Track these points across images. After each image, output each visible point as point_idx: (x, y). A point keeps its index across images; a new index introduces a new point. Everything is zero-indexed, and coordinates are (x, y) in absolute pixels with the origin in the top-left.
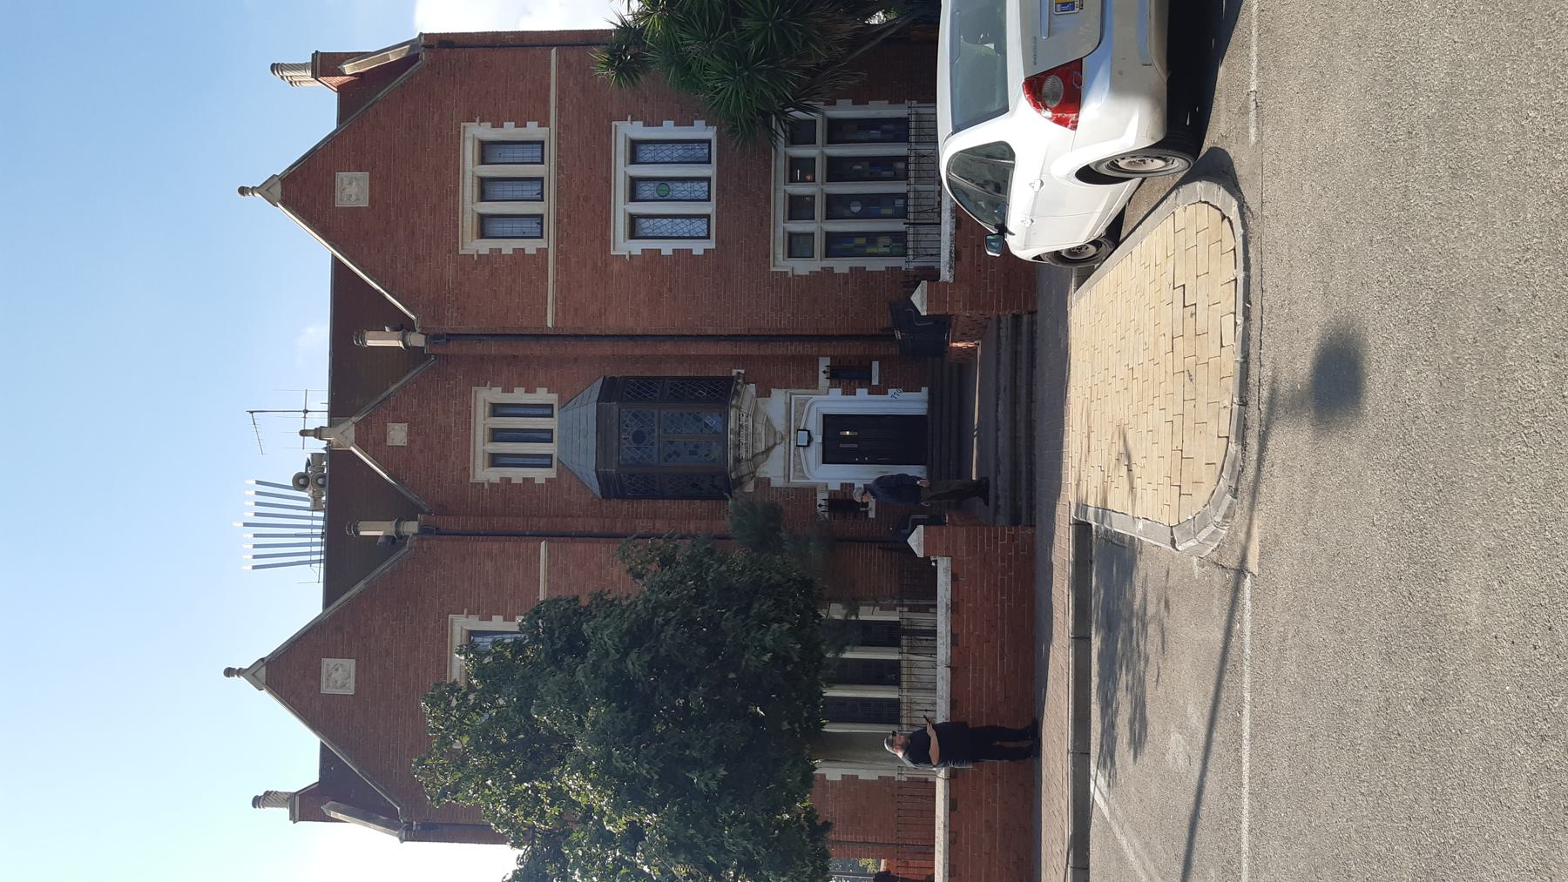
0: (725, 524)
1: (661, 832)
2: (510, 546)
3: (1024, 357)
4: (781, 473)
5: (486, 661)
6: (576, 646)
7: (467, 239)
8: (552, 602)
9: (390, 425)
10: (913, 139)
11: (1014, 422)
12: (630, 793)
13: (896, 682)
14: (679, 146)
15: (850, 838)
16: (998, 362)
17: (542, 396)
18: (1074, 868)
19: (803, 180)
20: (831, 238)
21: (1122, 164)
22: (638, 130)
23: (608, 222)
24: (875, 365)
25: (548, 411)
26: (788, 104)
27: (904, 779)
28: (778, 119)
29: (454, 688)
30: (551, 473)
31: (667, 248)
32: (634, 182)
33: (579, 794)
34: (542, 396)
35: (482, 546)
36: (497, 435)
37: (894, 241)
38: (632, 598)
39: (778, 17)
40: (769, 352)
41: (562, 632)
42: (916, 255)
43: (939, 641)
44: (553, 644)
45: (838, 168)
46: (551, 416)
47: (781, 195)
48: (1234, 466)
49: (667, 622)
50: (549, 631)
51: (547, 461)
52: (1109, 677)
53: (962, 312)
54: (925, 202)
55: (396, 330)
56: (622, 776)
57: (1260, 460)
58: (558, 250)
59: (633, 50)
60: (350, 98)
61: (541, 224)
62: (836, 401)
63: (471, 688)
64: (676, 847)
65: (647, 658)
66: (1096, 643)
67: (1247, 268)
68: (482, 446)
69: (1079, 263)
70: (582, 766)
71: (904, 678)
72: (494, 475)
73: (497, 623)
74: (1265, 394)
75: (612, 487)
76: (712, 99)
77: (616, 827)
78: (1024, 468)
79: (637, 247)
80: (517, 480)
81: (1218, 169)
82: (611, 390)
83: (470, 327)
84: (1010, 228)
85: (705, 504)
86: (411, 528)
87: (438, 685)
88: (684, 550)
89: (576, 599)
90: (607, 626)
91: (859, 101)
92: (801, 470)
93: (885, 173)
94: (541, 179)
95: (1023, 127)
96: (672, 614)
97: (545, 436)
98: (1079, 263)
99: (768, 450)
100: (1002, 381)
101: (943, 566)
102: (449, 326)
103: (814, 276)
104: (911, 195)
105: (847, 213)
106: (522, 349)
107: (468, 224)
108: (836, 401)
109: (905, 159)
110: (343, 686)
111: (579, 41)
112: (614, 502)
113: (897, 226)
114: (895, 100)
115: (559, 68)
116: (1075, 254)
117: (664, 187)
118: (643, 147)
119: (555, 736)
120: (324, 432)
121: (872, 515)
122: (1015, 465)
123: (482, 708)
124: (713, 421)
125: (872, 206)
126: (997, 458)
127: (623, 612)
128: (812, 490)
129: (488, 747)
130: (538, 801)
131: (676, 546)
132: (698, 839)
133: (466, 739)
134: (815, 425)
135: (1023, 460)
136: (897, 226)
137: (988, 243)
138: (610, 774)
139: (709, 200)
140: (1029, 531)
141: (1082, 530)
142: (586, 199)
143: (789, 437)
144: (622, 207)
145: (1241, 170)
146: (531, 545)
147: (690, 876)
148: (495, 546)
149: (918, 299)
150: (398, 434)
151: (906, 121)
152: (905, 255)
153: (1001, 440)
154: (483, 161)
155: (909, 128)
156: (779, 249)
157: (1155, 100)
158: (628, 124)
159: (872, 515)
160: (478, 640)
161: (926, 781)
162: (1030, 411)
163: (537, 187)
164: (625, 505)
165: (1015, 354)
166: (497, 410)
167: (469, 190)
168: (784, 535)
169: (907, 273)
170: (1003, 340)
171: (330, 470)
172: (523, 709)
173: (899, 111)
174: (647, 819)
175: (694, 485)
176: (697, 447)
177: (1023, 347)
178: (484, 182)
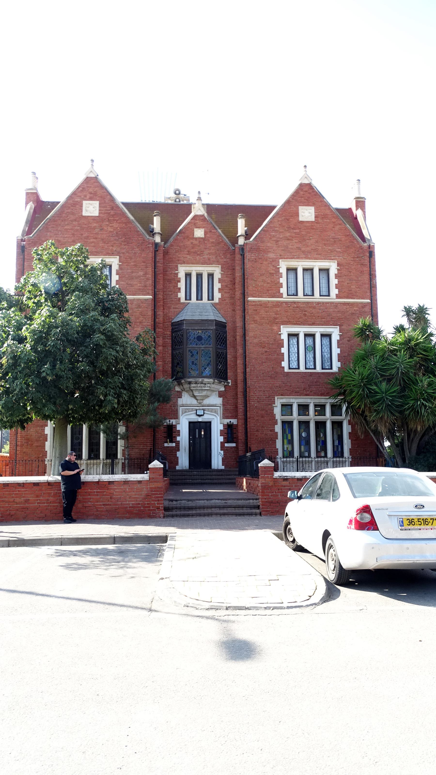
0: (161, 378)
1: (22, 352)
2: (150, 282)
3: (241, 511)
5: (99, 272)
6: (106, 311)
7: (287, 263)
8: (126, 301)
10: (335, 459)
11: (211, 507)
12: (40, 338)
13: (90, 458)
14: (329, 355)
15: (19, 438)
16: (238, 499)
17: (217, 296)
18: (9, 541)
19: (316, 411)
20: (291, 423)
21: (332, 550)
22: (336, 337)
23: (295, 324)
24: (234, 445)
25: (210, 298)
26: (349, 403)
27: (46, 463)
28: (342, 399)
29: (86, 258)
31: (284, 350)
32: (313, 336)
33: (39, 314)
34: (217, 296)
35: (150, 270)
36: (199, 276)
37: (290, 452)
38: (127, 336)
39: (387, 399)
40: (239, 396)
41: (111, 306)
42: (283, 462)
43: (111, 476)
44: (107, 301)
45: (320, 426)
46: (208, 300)
47: (309, 401)
48: (198, 605)
49: (117, 352)
50: (113, 300)
51: (188, 298)
52: (97, 553)
53: (259, 483)
54: (307, 465)
55: (246, 232)
56: (48, 333)
57: (202, 617)
58: (282, 303)
59: (371, 335)
60: (347, 214)
61: (294, 295)
62: (217, 427)
63: (86, 266)
64: (15, 359)
65: (101, 343)
66: (111, 547)
67: (288, 608)
68: (194, 270)
69: (285, 533)
70: (52, 315)
71: (92, 461)
72: (182, 275)
73: (115, 277)
74: (232, 618)
75: (177, 328)
76: (351, 369)
77: (24, 332)
78: (190, 512)
79: (284, 337)
81: (331, 594)
82: (221, 326)
83: (248, 265)
84: (300, 501)
85: (170, 369)
86: (158, 239)
87: (87, 251)
88: (150, 359)
89: (127, 311)
90: (115, 325)
91: (351, 435)
92: (185, 412)
93: (319, 447)
94: (313, 295)
95: (347, 505)
96: (121, 354)
97: (199, 297)
98: (285, 533)
99: (195, 397)
100: (229, 501)
101: (145, 477)
102: (248, 255)
103: (274, 416)
104: (310, 459)
105: (302, 430)
106: (238, 287)
107: (293, 263)
108: (217, 427)
109: (326, 456)
110: (86, 211)
112: (170, 328)
113: (296, 453)
115: (362, 303)
116: (289, 531)
117: (311, 349)
118: (328, 339)
119: (65, 303)
120: (200, 201)
121: (166, 445)
122: (196, 508)
123: (77, 271)
124: (208, 371)
126: (194, 500)
127: (122, 332)
128: (176, 417)
129: (60, 274)
130: (35, 297)
131: (150, 355)
132: (19, 369)
133: (64, 264)
134: (206, 418)
135: (194, 512)
136: (296, 453)
137: (293, 492)
138: (49, 328)
139: (306, 369)
140: (162, 515)
141: (164, 539)
142: (305, 315)
143: (201, 406)
144: (302, 330)
145: (331, 604)
146: (150, 292)
147: (2, 365)
148: (150, 276)
149: (266, 462)
150: (199, 233)
151: (342, 456)
152: (284, 457)
153: (203, 501)
154: (320, 270)
155: (339, 457)
156: (285, 400)
157: (361, 566)
158: (338, 333)
159: (166, 445)
160: (108, 269)
161: (45, 473)
162: (216, 514)
163: (310, 293)
164: (169, 333)
165: (242, 507)
166: (211, 276)
167: (308, 264)
168: (156, 404)
169: (275, 458)
170: (248, 501)
171: (182, 204)
172: (77, 289)
173: (346, 453)
174: (28, 345)
176: (196, 364)
177: (245, 511)
178: (311, 270)
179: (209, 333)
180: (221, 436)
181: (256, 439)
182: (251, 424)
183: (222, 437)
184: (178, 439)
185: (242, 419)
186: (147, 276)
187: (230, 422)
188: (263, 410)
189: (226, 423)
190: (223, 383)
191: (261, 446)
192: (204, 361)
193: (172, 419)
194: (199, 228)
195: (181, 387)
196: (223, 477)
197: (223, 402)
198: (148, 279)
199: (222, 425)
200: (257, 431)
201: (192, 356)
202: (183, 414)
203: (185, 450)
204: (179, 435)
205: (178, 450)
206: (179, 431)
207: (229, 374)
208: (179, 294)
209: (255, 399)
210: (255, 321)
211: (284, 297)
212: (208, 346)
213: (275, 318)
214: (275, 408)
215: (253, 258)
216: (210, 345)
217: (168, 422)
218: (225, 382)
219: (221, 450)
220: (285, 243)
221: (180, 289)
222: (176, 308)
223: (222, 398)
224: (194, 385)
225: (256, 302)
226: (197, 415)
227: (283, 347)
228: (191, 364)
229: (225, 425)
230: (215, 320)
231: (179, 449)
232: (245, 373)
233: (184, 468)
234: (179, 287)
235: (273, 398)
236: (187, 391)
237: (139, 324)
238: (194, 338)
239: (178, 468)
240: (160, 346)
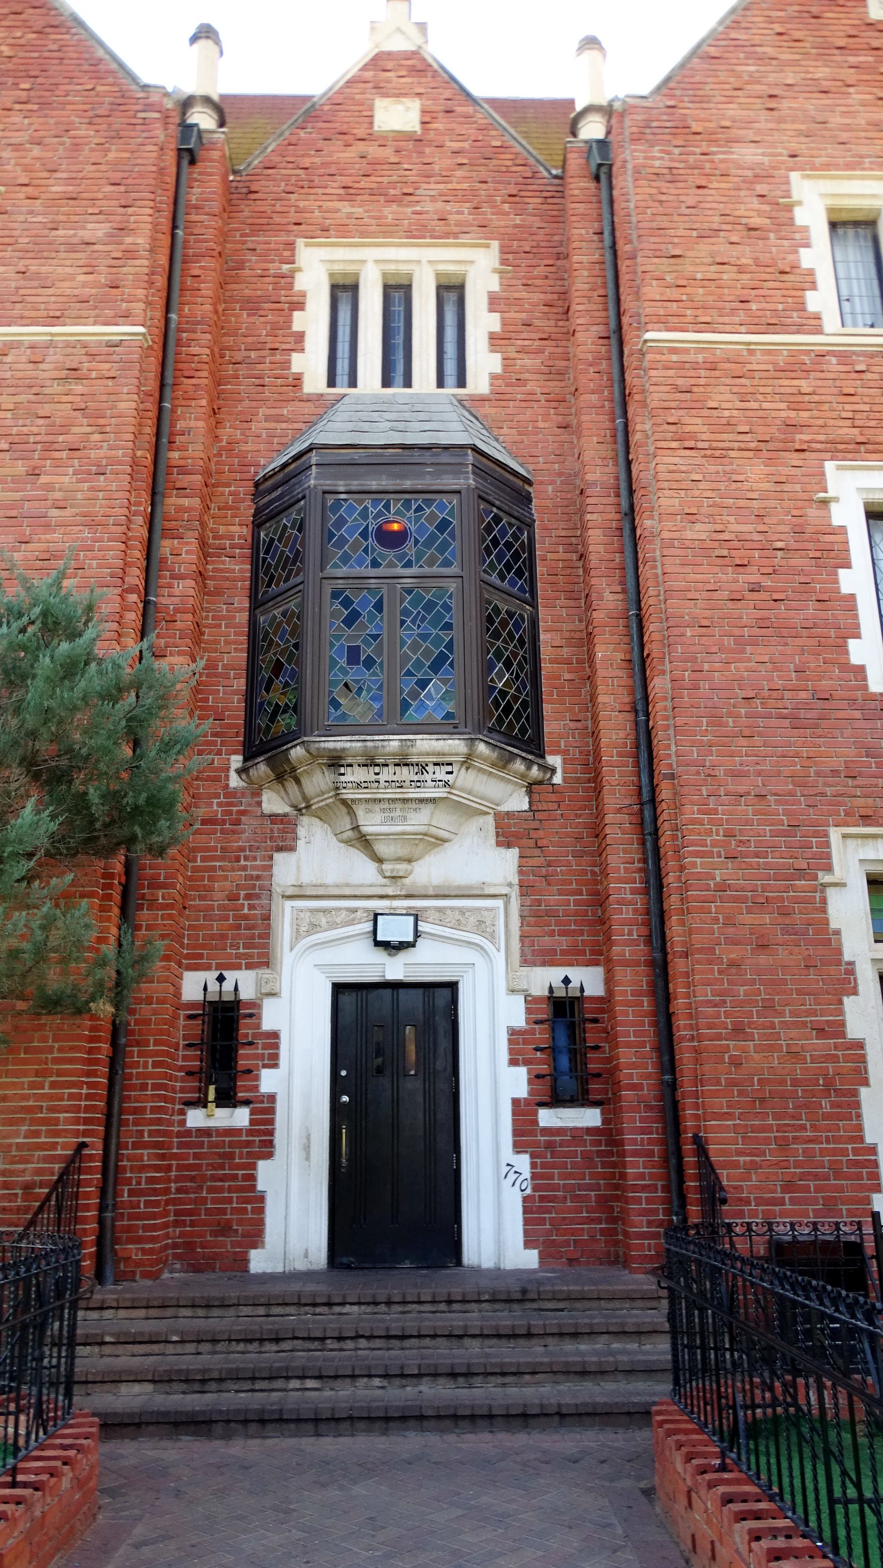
4: (307, 878)
17: (483, 365)
24: (589, 1117)
30: (315, 380)
34: (483, 365)
36: (398, 293)
68: (374, 264)
80: (299, 321)
85: (237, 703)
92: (314, 928)
97: (396, 366)
99: (363, 842)
103: (827, 942)
112: (247, 510)
121: (195, 1118)
124: (436, 699)
128: (261, 957)
159: (195, 1118)
166: (451, 292)
175: (278, 667)
176: (369, 663)
179: (441, 507)
180: (513, 1062)
181: (732, 1083)
182: (699, 991)
183: (522, 1072)
184: (269, 1081)
185: (637, 963)
186: (129, 240)
187: (566, 981)
188: (760, 905)
189: (539, 990)
190: (519, 766)
191: (769, 1129)
192: (415, 647)
193: (238, 967)
194: (398, 96)
195: (291, 786)
196: (535, 1352)
197: (521, 872)
198: (130, 254)
199: (520, 1000)
200: (738, 1031)
201: (350, 621)
202: (297, 936)
203: (307, 1148)
204: (273, 1062)
205: (267, 1149)
206: (275, 1035)
207: (550, 727)
208: (295, 356)
209: (714, 844)
210: (688, 443)
211: (827, 329)
212: (435, 570)
213: (791, 426)
214: (832, 895)
215: (657, 163)
216: (447, 563)
217: (213, 986)
218: (529, 764)
219: (519, 1147)
220: (812, 105)
221: (300, 337)
222: (279, 419)
223: (515, 852)
224: (357, 774)
225: (686, 351)
226: (377, 944)
227: (848, 566)
228: (343, 662)
229: (537, 1000)
230: (475, 449)
231: (271, 1144)
232: (641, 706)
233: (300, 1265)
234: (296, 327)
235: (816, 834)
236: (322, 815)
237: (64, 454)
238: (364, 534)
239: (260, 1261)
240: (181, 577)
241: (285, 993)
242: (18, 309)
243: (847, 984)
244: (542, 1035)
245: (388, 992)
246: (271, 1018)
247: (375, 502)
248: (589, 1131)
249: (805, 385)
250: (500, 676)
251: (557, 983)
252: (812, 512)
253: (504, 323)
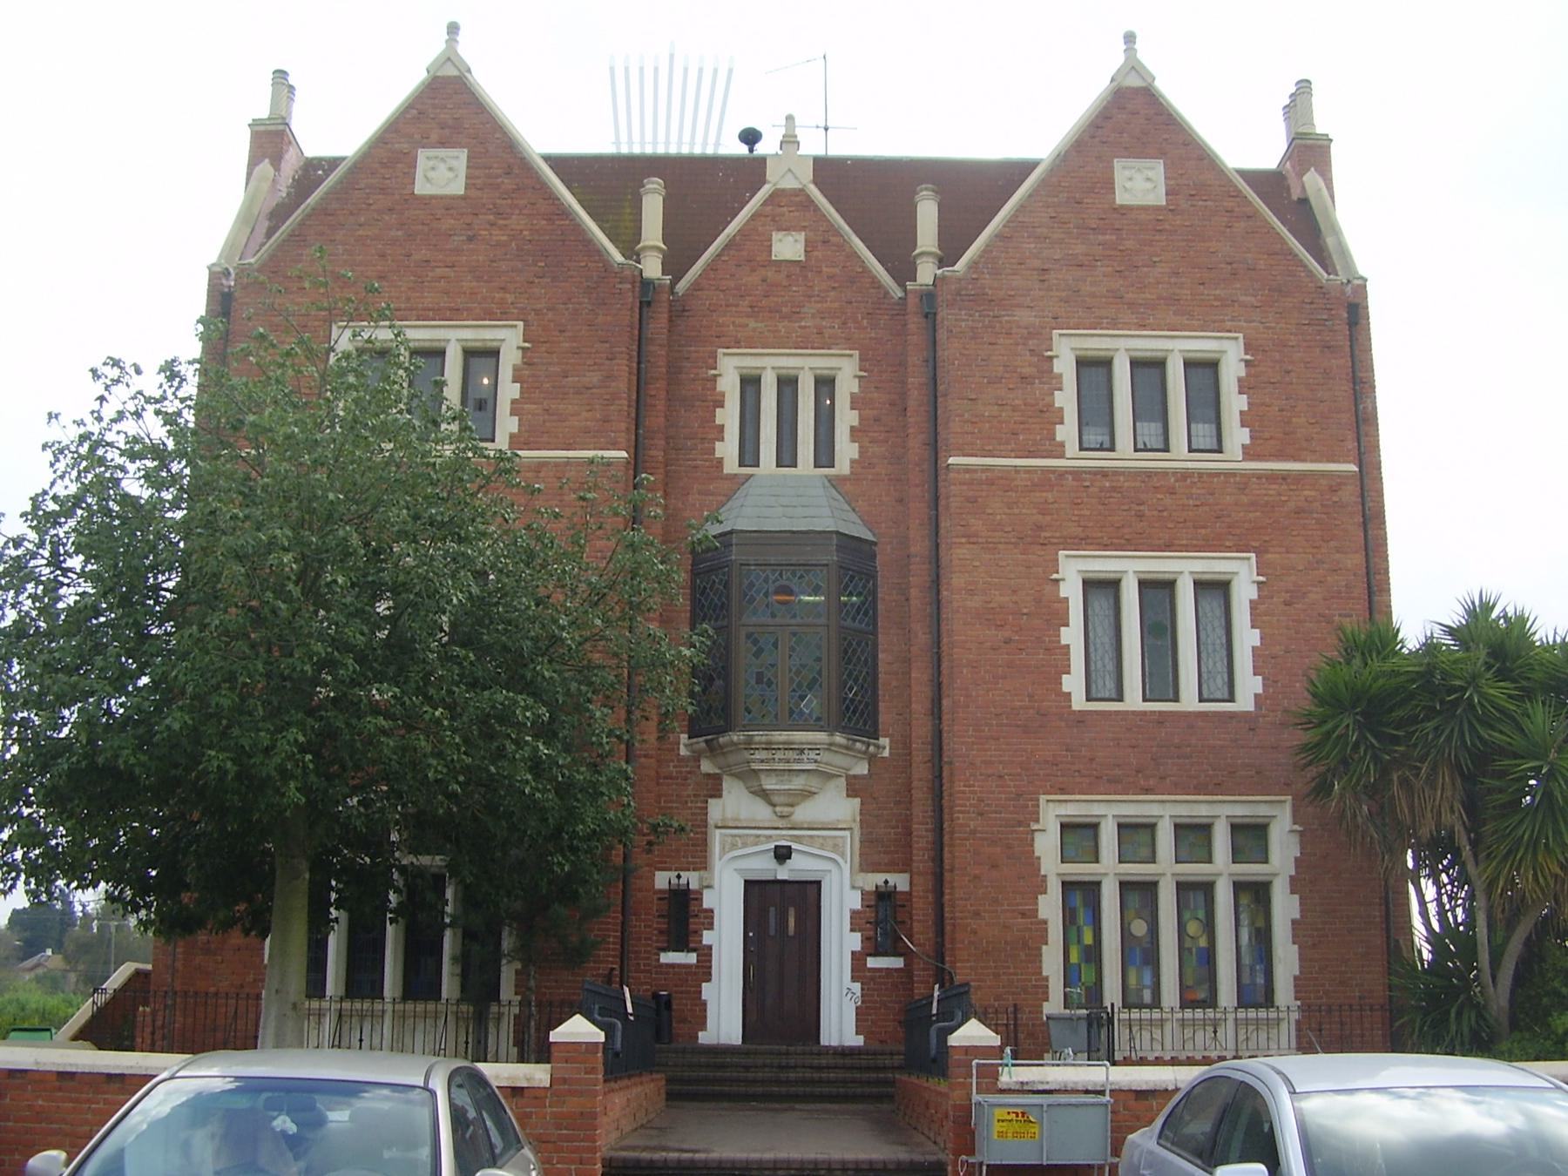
9: (801, 237)
17: (846, 451)
23: (1106, 547)
24: (897, 963)
31: (1072, 636)
34: (846, 451)
35: (623, 368)
47: (1155, 810)
54: (1146, 1035)
58: (1061, 474)
60: (1269, 184)
61: (1101, 449)
62: (842, 900)
68: (770, 365)
72: (729, 384)
80: (721, 416)
92: (734, 846)
97: (786, 456)
99: (764, 795)
103: (1033, 863)
104: (1156, 1015)
106: (916, 419)
107: (1096, 343)
108: (842, 900)
111: (1369, 504)
114: (1300, 985)
124: (811, 704)
125: (1140, 953)
128: (700, 860)
134: (800, 867)
142: (1140, 516)
144: (1130, 567)
146: (622, 438)
148: (623, 385)
150: (788, 247)
155: (1257, 1006)
156: (1075, 809)
159: (668, 958)
166: (825, 384)
167: (1148, 344)
173: (1284, 992)
178: (1159, 365)
182: (959, 892)
184: (708, 937)
187: (886, 882)
200: (977, 914)
202: (723, 852)
204: (710, 927)
205: (708, 977)
213: (1040, 528)
223: (858, 800)
225: (975, 471)
228: (753, 682)
230: (837, 533)
241: (716, 885)
242: (545, 439)
243: (1042, 889)
244: (871, 914)
245: (778, 887)
246: (708, 901)
247: (774, 571)
248: (897, 970)
249: (1050, 496)
250: (851, 689)
251: (881, 883)
252: (1048, 588)
253: (861, 418)
